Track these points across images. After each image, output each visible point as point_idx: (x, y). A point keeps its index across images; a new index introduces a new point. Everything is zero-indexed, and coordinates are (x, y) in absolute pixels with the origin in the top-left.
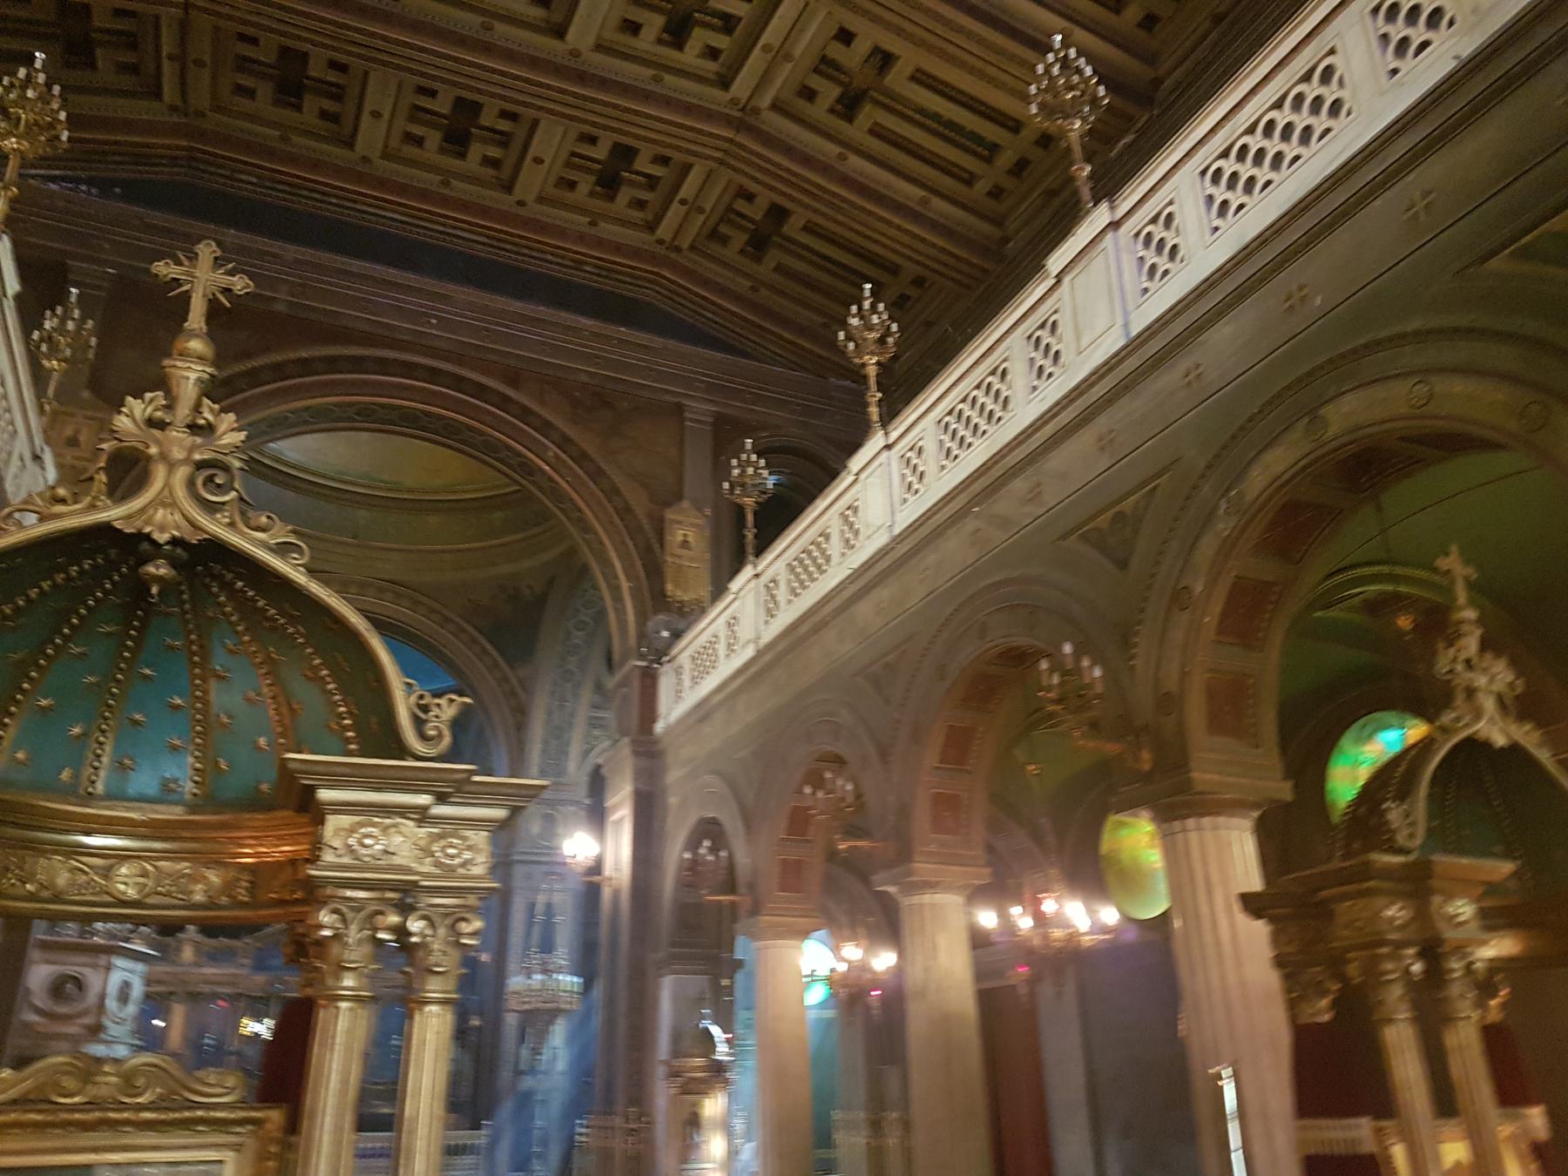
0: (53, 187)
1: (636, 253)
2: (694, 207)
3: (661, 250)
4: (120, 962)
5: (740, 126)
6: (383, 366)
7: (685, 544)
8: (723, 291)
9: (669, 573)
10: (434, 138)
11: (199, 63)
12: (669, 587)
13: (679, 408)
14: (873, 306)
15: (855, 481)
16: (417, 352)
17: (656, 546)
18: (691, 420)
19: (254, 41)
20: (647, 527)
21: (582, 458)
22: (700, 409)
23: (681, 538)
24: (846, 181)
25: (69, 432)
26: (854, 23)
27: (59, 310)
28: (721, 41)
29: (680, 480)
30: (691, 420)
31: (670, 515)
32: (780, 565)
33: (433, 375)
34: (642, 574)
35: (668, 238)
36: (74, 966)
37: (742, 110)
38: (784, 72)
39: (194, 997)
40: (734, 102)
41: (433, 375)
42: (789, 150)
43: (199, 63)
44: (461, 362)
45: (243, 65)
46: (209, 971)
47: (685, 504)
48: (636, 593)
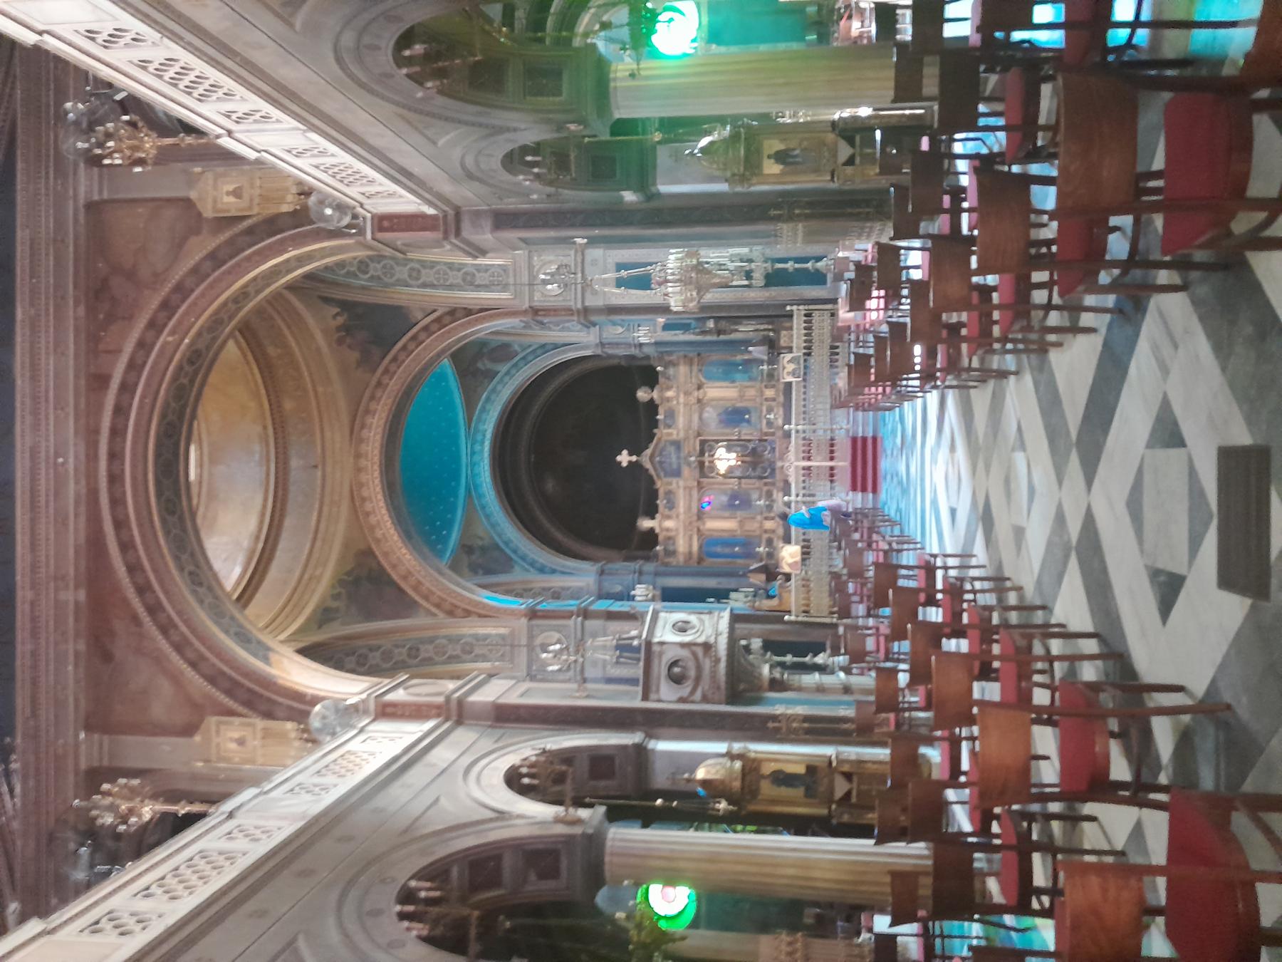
0: (18, 789)
6: (117, 502)
7: (237, 193)
9: (272, 210)
12: (285, 208)
13: (91, 207)
15: (48, 32)
16: (96, 469)
18: (101, 192)
20: (227, 235)
21: (168, 307)
23: (232, 199)
25: (233, 746)
27: (94, 813)
29: (169, 201)
30: (101, 192)
31: (208, 213)
32: (203, 108)
33: (115, 456)
36: (660, 669)
39: (700, 516)
41: (115, 456)
44: (97, 432)
46: (681, 510)
47: (193, 195)
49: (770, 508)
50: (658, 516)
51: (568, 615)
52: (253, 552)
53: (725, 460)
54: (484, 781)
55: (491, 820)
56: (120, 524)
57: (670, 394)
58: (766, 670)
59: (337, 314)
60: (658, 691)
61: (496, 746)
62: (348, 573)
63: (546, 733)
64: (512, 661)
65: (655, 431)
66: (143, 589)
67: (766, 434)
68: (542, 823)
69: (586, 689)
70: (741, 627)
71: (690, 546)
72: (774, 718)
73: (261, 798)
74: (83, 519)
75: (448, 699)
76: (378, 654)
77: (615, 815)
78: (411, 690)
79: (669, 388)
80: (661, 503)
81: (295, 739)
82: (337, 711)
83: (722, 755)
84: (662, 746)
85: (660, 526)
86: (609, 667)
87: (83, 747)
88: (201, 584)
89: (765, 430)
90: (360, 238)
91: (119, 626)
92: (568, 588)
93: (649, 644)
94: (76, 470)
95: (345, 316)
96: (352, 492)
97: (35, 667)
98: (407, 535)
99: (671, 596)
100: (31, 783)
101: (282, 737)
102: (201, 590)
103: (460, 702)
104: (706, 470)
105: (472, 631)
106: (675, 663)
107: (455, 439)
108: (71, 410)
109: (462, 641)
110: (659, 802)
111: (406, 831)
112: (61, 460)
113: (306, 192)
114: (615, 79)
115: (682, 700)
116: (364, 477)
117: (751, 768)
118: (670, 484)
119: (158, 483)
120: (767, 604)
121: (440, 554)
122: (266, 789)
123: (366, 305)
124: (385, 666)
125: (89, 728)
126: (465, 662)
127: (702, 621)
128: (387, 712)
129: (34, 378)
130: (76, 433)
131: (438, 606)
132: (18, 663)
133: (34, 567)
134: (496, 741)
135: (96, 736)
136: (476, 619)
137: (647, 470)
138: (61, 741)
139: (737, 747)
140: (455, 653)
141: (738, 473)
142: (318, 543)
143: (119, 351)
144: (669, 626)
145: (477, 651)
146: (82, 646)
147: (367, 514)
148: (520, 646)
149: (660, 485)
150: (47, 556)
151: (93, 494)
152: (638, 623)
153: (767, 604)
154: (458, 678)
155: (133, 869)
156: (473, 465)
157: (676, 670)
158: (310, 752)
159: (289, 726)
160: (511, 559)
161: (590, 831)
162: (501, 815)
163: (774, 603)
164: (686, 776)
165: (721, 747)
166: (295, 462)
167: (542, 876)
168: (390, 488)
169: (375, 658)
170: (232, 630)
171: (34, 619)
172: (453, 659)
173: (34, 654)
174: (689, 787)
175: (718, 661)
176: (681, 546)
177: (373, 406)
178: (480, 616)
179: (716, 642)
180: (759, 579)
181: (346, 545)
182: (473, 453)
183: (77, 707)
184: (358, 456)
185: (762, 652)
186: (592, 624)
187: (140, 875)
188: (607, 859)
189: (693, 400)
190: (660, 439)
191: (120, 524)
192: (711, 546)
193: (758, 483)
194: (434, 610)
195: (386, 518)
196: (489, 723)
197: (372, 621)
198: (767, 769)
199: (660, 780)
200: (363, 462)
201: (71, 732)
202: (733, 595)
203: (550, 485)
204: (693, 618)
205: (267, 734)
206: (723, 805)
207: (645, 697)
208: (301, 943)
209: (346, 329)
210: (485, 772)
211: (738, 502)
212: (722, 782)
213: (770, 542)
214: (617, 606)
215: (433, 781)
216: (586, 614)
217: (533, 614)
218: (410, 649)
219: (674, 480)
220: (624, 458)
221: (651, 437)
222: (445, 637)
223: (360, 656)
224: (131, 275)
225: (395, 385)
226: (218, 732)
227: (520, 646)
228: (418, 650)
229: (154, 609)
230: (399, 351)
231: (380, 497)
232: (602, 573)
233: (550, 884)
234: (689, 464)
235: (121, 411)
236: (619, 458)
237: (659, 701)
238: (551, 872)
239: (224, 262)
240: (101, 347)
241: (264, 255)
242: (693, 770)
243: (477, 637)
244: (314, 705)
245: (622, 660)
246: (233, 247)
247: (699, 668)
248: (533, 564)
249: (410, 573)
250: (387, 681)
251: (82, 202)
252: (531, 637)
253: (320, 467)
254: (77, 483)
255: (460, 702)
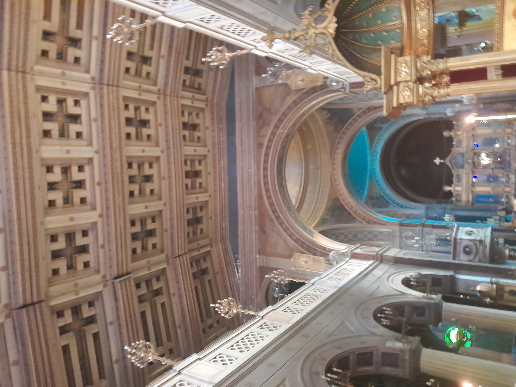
0: (240, 271)
1: (212, 112)
2: (193, 99)
3: (209, 104)
4: (459, 237)
5: (165, 95)
6: (266, 183)
7: (303, 80)
8: (215, 81)
9: (314, 85)
10: (198, 180)
11: (198, 244)
13: (257, 89)
14: (210, 57)
17: (304, 91)
19: (188, 233)
21: (280, 120)
22: (255, 82)
23: (301, 83)
24: (170, 53)
25: (303, 263)
26: (123, 70)
28: (143, 109)
31: (293, 88)
33: (265, 169)
34: (316, 94)
35: (205, 103)
36: (460, 248)
37: (160, 94)
38: (144, 86)
40: (159, 98)
41: (265, 169)
42: (167, 76)
43: (198, 244)
44: (260, 162)
45: (195, 233)
48: (322, 95)
49: (508, 182)
50: (453, 185)
51: (416, 226)
52: (298, 198)
53: (485, 160)
54: (394, 282)
55: (400, 295)
56: (267, 191)
57: (459, 133)
58: (507, 252)
59: (326, 114)
60: (459, 256)
61: (396, 271)
62: (331, 206)
63: (414, 268)
64: (393, 242)
65: (452, 149)
66: (274, 211)
67: (506, 149)
68: (418, 298)
69: (429, 254)
70: (496, 234)
71: (468, 198)
72: (511, 270)
73: (320, 280)
74: (256, 189)
75: (377, 254)
76: (342, 236)
77: (446, 299)
78: (364, 250)
79: (459, 130)
80: (454, 180)
81: (324, 263)
82: (338, 254)
83: (488, 282)
84: (462, 277)
85: (454, 190)
86: (433, 247)
87: (258, 260)
88: (290, 210)
89: (506, 146)
90: (345, 92)
91: (267, 222)
92: (413, 214)
93: (455, 239)
94: (254, 174)
95: (330, 114)
96: (331, 177)
97: (244, 234)
98: (350, 192)
99: (459, 219)
100: (244, 269)
101: (319, 262)
102: (291, 212)
103: (382, 255)
104: (476, 166)
105: (378, 230)
106: (467, 247)
107: (365, 156)
108: (252, 155)
109: (373, 233)
110: (461, 296)
111: (371, 295)
112: (249, 171)
113: (326, 78)
114: (449, 33)
115: (469, 261)
116: (335, 172)
117: (500, 288)
118: (459, 171)
119: (278, 178)
120: (506, 224)
121: (361, 199)
122: (321, 277)
123: (337, 109)
124: (345, 240)
125: (259, 254)
126: (374, 241)
127: (478, 232)
128: (355, 256)
129: (242, 145)
130: (254, 162)
131: (363, 220)
132: (239, 232)
133: (243, 203)
134: (397, 269)
135: (262, 257)
136: (379, 225)
137: (447, 166)
138: (252, 257)
139: (494, 280)
140: (370, 237)
141: (492, 166)
142: (320, 196)
143: (265, 136)
144: (464, 233)
145: (379, 237)
146: (257, 228)
147: (337, 185)
148: (396, 236)
149: (454, 173)
150: (247, 200)
151: (259, 181)
152: (450, 230)
153: (506, 224)
154: (381, 246)
155: (290, 296)
156: (373, 165)
157: (467, 249)
158: (329, 268)
159: (322, 258)
160: (388, 202)
161: (437, 302)
162: (403, 293)
163: (510, 224)
164: (472, 288)
165: (488, 279)
166: (311, 167)
167: (419, 315)
168: (344, 176)
169: (342, 237)
170: (301, 225)
171: (243, 219)
172: (370, 239)
173: (244, 230)
174: (474, 293)
175: (486, 247)
176: (464, 198)
177: (339, 146)
178: (380, 224)
179: (485, 240)
180: (503, 213)
181: (329, 196)
182: (373, 160)
183: (256, 248)
184: (333, 164)
185: (503, 244)
186: (426, 229)
187: (293, 298)
188: (443, 313)
189: (470, 135)
190: (454, 153)
191: (267, 191)
192: (478, 198)
193: (502, 171)
194: (361, 221)
195: (344, 187)
196: (392, 263)
197: (339, 224)
198: (507, 289)
199: (461, 288)
200: (335, 166)
201: (254, 255)
202: (489, 220)
203: (403, 171)
204: (474, 230)
205: (314, 260)
206: (488, 300)
207: (454, 258)
208: (346, 322)
209: (330, 119)
210: (394, 279)
211: (492, 179)
212: (488, 292)
213: (507, 197)
214: (437, 223)
215: (376, 281)
216: (423, 225)
217: (401, 225)
218: (354, 235)
219: (461, 170)
220: (437, 161)
221: (449, 152)
222: (366, 231)
223: (336, 236)
224: (269, 110)
225: (346, 138)
226: (299, 258)
227: (396, 236)
228: (357, 235)
229: (278, 218)
230: (348, 125)
231: (341, 179)
232: (427, 208)
233: (421, 318)
234: (468, 163)
235: (267, 155)
236: (435, 161)
237: (460, 260)
238: (422, 314)
239: (298, 104)
240: (261, 134)
241: (311, 100)
242: (475, 286)
243: (379, 232)
244: (330, 252)
245: (440, 244)
246: (301, 99)
247: (477, 249)
248: (398, 204)
249: (352, 207)
250: (353, 246)
251: (254, 87)
252: (401, 233)
253: (320, 169)
254: (255, 177)
255: (382, 255)
